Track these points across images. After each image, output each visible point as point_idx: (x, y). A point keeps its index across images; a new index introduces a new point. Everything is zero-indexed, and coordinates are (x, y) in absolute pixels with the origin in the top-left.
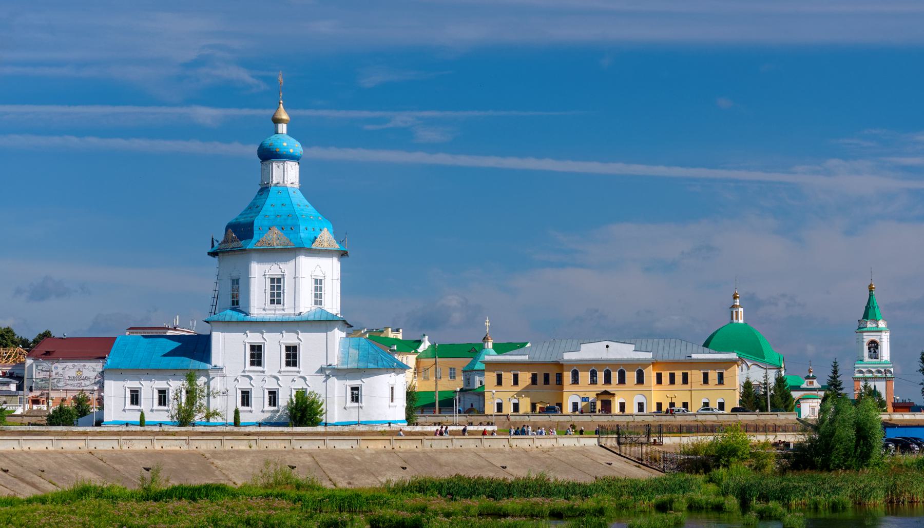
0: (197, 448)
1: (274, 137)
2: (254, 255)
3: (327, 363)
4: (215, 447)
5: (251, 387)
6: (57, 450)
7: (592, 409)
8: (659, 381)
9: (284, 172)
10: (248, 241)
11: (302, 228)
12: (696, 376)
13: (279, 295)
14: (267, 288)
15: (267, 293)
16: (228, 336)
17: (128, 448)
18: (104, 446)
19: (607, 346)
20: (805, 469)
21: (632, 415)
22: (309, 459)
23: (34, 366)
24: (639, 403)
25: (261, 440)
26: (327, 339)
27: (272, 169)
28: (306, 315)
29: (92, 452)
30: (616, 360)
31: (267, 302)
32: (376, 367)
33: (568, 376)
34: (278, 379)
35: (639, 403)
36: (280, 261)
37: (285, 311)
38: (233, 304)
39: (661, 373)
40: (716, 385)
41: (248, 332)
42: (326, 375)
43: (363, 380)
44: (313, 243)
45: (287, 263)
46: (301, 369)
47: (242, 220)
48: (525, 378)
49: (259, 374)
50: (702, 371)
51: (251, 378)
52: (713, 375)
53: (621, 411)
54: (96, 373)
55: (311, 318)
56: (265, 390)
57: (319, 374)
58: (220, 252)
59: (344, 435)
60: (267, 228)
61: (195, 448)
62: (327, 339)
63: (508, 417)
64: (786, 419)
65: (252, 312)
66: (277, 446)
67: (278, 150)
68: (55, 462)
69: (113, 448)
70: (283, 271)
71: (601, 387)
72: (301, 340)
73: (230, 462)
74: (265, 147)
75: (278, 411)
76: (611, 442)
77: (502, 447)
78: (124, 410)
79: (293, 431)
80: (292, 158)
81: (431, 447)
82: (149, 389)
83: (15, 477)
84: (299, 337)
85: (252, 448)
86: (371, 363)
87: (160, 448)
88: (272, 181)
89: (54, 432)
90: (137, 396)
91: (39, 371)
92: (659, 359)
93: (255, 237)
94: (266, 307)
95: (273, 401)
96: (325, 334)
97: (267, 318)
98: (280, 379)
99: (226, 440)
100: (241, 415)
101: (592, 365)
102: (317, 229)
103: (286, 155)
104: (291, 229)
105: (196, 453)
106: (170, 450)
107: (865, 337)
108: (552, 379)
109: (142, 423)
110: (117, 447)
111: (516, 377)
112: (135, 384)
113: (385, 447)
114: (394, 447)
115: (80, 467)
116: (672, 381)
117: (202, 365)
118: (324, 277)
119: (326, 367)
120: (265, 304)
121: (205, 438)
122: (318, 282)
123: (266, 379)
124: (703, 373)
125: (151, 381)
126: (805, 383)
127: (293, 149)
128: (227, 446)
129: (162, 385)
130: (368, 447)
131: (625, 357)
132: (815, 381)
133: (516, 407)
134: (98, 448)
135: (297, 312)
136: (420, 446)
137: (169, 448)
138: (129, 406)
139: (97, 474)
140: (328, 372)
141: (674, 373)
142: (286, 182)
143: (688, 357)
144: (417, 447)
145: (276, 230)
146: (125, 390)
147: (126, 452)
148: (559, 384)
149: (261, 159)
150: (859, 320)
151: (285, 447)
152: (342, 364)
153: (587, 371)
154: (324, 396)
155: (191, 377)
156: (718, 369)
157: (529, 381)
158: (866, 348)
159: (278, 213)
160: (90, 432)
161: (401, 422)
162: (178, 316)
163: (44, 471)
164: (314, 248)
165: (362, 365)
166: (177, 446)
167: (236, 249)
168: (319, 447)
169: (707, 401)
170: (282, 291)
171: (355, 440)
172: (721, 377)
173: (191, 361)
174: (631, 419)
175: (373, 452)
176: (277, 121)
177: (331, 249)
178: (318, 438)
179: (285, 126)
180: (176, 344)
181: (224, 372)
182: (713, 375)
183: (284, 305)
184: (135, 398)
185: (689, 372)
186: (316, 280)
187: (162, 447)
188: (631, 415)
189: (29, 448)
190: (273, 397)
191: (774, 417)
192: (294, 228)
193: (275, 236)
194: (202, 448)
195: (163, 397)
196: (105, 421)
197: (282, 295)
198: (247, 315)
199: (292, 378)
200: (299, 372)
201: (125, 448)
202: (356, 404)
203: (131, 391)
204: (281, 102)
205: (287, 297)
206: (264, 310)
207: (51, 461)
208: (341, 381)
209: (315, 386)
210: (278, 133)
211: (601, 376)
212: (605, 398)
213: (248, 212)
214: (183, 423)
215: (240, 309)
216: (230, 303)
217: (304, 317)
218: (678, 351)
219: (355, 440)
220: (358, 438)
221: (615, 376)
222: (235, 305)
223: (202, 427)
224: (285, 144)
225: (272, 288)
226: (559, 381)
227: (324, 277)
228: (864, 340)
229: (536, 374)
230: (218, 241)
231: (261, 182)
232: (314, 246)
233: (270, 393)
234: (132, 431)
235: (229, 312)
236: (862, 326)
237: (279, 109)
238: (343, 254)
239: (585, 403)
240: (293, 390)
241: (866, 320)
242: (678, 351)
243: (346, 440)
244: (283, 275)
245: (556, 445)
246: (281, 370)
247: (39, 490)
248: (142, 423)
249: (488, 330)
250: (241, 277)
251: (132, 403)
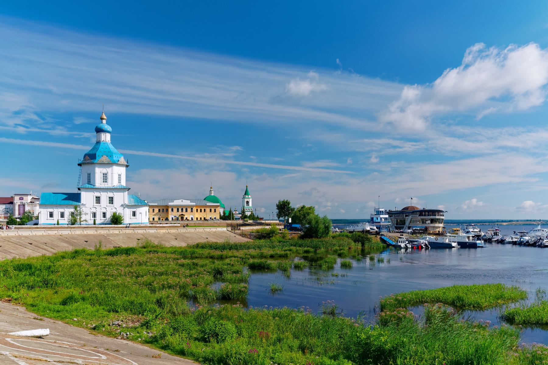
1: (101, 124)
2: (97, 165)
7: (177, 219)
10: (94, 160)
11: (114, 156)
12: (208, 210)
13: (106, 179)
19: (182, 201)
20: (315, 238)
22: (142, 236)
30: (185, 205)
33: (170, 210)
34: (106, 208)
36: (107, 167)
37: (109, 185)
48: (156, 210)
49: (99, 207)
51: (96, 208)
52: (213, 210)
53: (153, 220)
55: (118, 188)
59: (137, 228)
64: (239, 222)
71: (180, 213)
72: (101, 195)
73: (115, 238)
75: (106, 220)
76: (230, 229)
78: (47, 219)
80: (108, 132)
82: (57, 212)
83: (36, 246)
87: (86, 233)
93: (97, 158)
94: (102, 183)
97: (102, 187)
100: (59, 221)
101: (172, 206)
102: (119, 157)
108: (165, 210)
110: (70, 233)
111: (153, 210)
112: (51, 210)
117: (77, 203)
122: (120, 175)
128: (111, 232)
131: (187, 204)
132: (237, 212)
133: (154, 219)
135: (113, 185)
137: (90, 233)
140: (124, 206)
154: (123, 214)
158: (245, 203)
165: (136, 204)
172: (215, 210)
176: (102, 119)
179: (105, 121)
180: (65, 196)
182: (213, 210)
184: (51, 215)
186: (119, 175)
190: (104, 215)
192: (111, 156)
195: (62, 215)
198: (94, 186)
200: (114, 206)
201: (73, 233)
202: (134, 217)
205: (109, 180)
206: (101, 184)
209: (120, 211)
212: (182, 216)
214: (73, 224)
216: (87, 182)
217: (116, 187)
220: (157, 228)
221: (184, 210)
222: (89, 182)
223: (134, 225)
224: (106, 127)
225: (104, 177)
232: (119, 163)
233: (103, 213)
235: (87, 185)
238: (127, 166)
239: (175, 218)
244: (108, 173)
251: (50, 217)
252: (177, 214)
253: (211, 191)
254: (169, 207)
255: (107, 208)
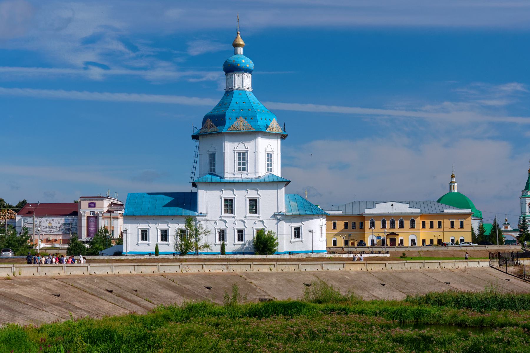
0: (234, 271)
1: (234, 56)
2: (227, 137)
3: (278, 211)
4: (247, 270)
5: (226, 228)
6: (138, 273)
8: (424, 226)
9: (243, 80)
11: (259, 118)
12: (446, 223)
13: (244, 164)
14: (236, 160)
15: (236, 163)
16: (209, 192)
17: (187, 271)
18: (125, 270)
19: (392, 205)
21: (408, 247)
22: (314, 278)
23: (22, 220)
24: (412, 240)
25: (278, 264)
26: (278, 194)
27: (235, 78)
28: (263, 178)
29: (163, 275)
30: (398, 214)
31: (236, 170)
32: (312, 214)
33: (368, 224)
34: (244, 222)
35: (412, 240)
36: (245, 141)
37: (249, 175)
38: (211, 171)
39: (425, 222)
40: (459, 228)
41: (223, 190)
42: (278, 220)
43: (302, 222)
44: (267, 129)
45: (250, 142)
46: (260, 215)
47: (216, 113)
48: (341, 225)
50: (450, 220)
51: (225, 222)
52: (457, 223)
54: (60, 225)
55: (267, 180)
56: (236, 230)
57: (273, 219)
58: (200, 135)
60: (235, 118)
61: (232, 271)
62: (278, 194)
63: (342, 249)
65: (226, 176)
66: (289, 269)
67: (239, 65)
68: (142, 283)
69: (176, 271)
70: (247, 148)
71: (388, 230)
73: (262, 281)
74: (229, 63)
75: (245, 244)
76: (496, 264)
77: (436, 268)
78: (137, 244)
79: (268, 258)
80: (248, 71)
81: (392, 268)
83: (119, 296)
84: (259, 193)
85: (272, 271)
86: (308, 211)
87: (208, 272)
88: (235, 87)
89: (99, 259)
90: (146, 234)
91: (25, 223)
92: (424, 213)
93: (227, 124)
95: (222, 238)
96: (277, 191)
97: (236, 180)
98: (246, 222)
99: (254, 264)
103: (244, 68)
104: (252, 119)
105: (235, 275)
106: (215, 273)
107: (527, 201)
108: (358, 225)
109: (157, 253)
110: (179, 271)
112: (144, 226)
113: (362, 269)
114: (367, 269)
115: (161, 287)
116: (432, 226)
118: (273, 152)
119: (277, 213)
120: (235, 171)
121: (239, 263)
122: (269, 155)
123: (236, 222)
124: (451, 221)
125: (156, 224)
126: (503, 227)
127: (249, 65)
129: (164, 226)
130: (350, 269)
131: (403, 212)
132: (509, 227)
134: (166, 272)
135: (257, 176)
136: (403, 267)
137: (214, 271)
138: (140, 241)
139: (176, 293)
140: (279, 217)
141: (433, 222)
142: (244, 87)
143: (442, 211)
144: (382, 269)
145: (242, 119)
146: (138, 230)
147: (187, 274)
148: (354, 229)
149: (225, 72)
150: (522, 191)
151: (294, 270)
152: (288, 212)
153: (408, 220)
155: (189, 221)
156: (460, 219)
157: (343, 227)
159: (241, 109)
160: (124, 259)
161: (323, 251)
162: (109, 190)
163: (137, 291)
164: (268, 132)
165: (302, 212)
166: (220, 269)
167: (214, 132)
168: (317, 270)
169: (463, 238)
170: (246, 162)
171: (296, 264)
173: (183, 210)
174: (407, 249)
175: (355, 273)
176: (236, 46)
177: (278, 133)
178: (317, 263)
179: (242, 49)
181: (207, 217)
182: (457, 223)
183: (247, 171)
184: (145, 236)
185: (442, 221)
187: (210, 271)
188: (420, 247)
189: (118, 272)
190: (241, 234)
191: (508, 248)
192: (253, 118)
193: (241, 123)
194: (238, 271)
195: (164, 236)
196: (124, 252)
197: (246, 164)
198: (222, 178)
199: (254, 221)
200: (259, 217)
201: (185, 271)
203: (142, 231)
204: (239, 32)
205: (250, 166)
206: (234, 174)
207: (139, 283)
208: (288, 223)
210: (237, 54)
211: (388, 224)
213: (219, 108)
214: (183, 253)
215: (216, 174)
217: (262, 179)
218: (433, 208)
219: (296, 264)
221: (397, 223)
222: (212, 172)
224: (243, 61)
225: (239, 159)
226: (354, 227)
227: (273, 152)
228: (527, 203)
229: (348, 222)
230: (196, 128)
231: (226, 88)
232: (268, 130)
233: (239, 232)
234: (154, 259)
235: (209, 176)
236: (524, 194)
237: (238, 37)
238: (283, 137)
240: (255, 230)
241: (527, 191)
242: (433, 208)
243: (263, 264)
244: (247, 151)
245: (467, 267)
246: (246, 216)
247: (141, 307)
248: (157, 253)
249: (306, 197)
250: (216, 152)
251: (143, 239)
252: (383, 233)
253: (452, 182)
254: (366, 218)
255: (246, 221)
